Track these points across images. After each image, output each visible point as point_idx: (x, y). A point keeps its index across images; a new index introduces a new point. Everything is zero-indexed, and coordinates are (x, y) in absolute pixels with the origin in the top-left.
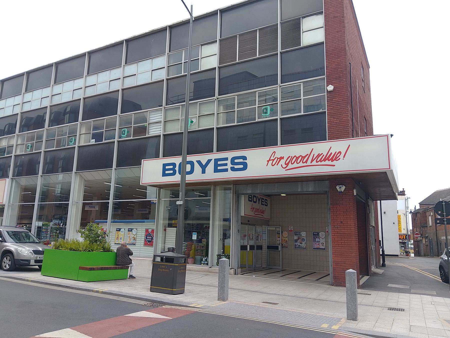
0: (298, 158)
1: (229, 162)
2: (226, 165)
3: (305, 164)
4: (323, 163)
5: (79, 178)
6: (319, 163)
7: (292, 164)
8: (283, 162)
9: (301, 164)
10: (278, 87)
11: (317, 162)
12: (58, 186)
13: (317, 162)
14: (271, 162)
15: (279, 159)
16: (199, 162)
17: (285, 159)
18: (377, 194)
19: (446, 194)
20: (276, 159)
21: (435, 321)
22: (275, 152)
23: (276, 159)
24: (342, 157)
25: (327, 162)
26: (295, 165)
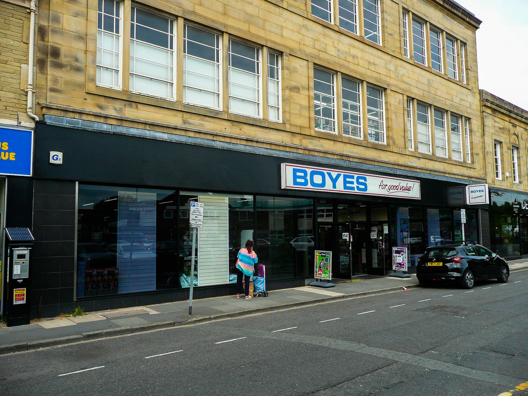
0: (394, 187)
1: (355, 180)
2: (352, 183)
3: (397, 191)
4: (405, 191)
5: (175, 192)
6: (403, 191)
7: (392, 190)
8: (387, 187)
9: (396, 190)
10: (360, 137)
11: (402, 190)
12: (473, 281)
13: (402, 190)
14: (381, 186)
15: (385, 186)
16: (329, 175)
17: (388, 186)
18: (185, 250)
19: (209, 242)
20: (384, 185)
21: (491, 167)
22: (382, 181)
23: (384, 185)
24: (411, 189)
25: (406, 191)
26: (393, 191)
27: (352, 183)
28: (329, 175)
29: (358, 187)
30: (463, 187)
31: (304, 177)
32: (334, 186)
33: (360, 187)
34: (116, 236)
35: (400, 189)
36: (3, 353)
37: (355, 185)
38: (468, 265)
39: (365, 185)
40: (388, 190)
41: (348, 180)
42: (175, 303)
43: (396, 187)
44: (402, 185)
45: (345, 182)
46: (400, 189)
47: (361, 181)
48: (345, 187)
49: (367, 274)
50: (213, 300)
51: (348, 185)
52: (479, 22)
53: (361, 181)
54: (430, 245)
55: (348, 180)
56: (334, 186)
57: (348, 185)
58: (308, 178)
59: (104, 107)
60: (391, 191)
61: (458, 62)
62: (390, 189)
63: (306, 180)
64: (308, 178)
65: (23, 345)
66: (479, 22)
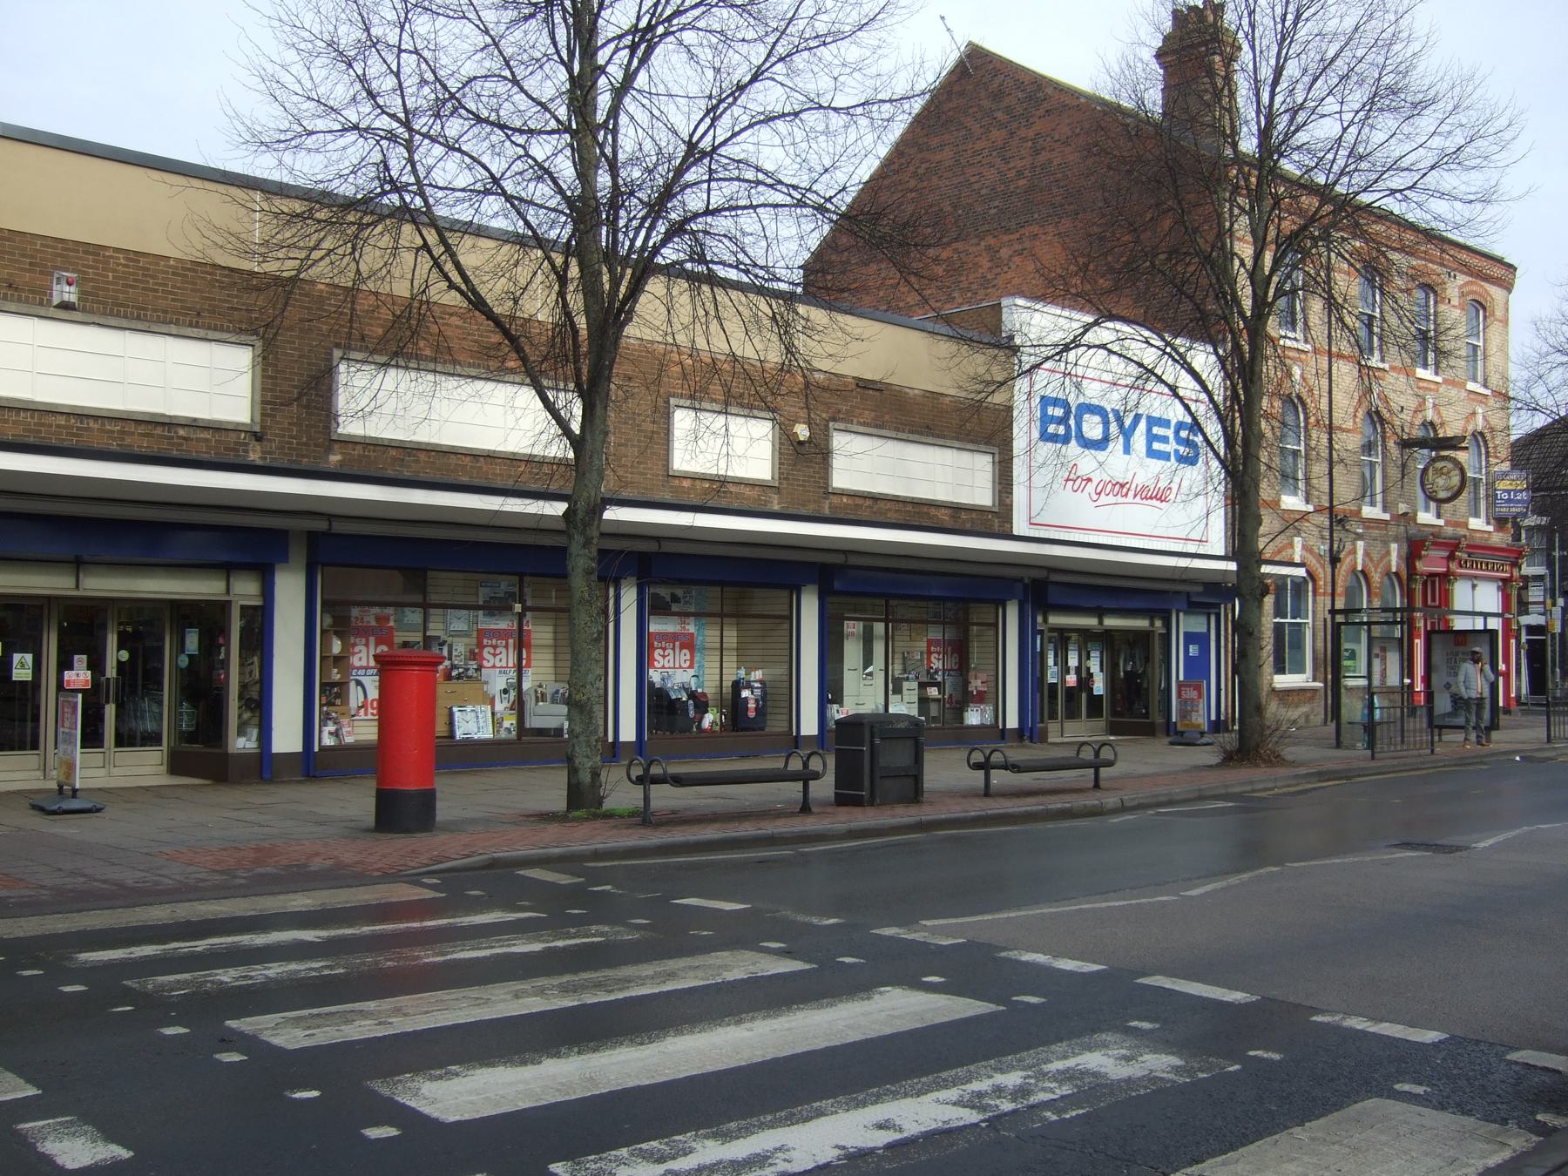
1: (1170, 433)
2: (1165, 440)
6: (1145, 502)
8: (1091, 487)
17: (1095, 481)
23: (1079, 480)
24: (1172, 497)
25: (1154, 502)
27: (1165, 440)
35: (1135, 496)
36: (1082, 100)
38: (280, 1051)
41: (1155, 430)
45: (1151, 438)
46: (1135, 496)
49: (163, 639)
50: (590, 1090)
51: (1156, 446)
52: (1515, 269)
55: (1155, 430)
57: (1156, 446)
59: (1493, 183)
63: (1068, 427)
64: (1072, 422)
66: (1511, 268)
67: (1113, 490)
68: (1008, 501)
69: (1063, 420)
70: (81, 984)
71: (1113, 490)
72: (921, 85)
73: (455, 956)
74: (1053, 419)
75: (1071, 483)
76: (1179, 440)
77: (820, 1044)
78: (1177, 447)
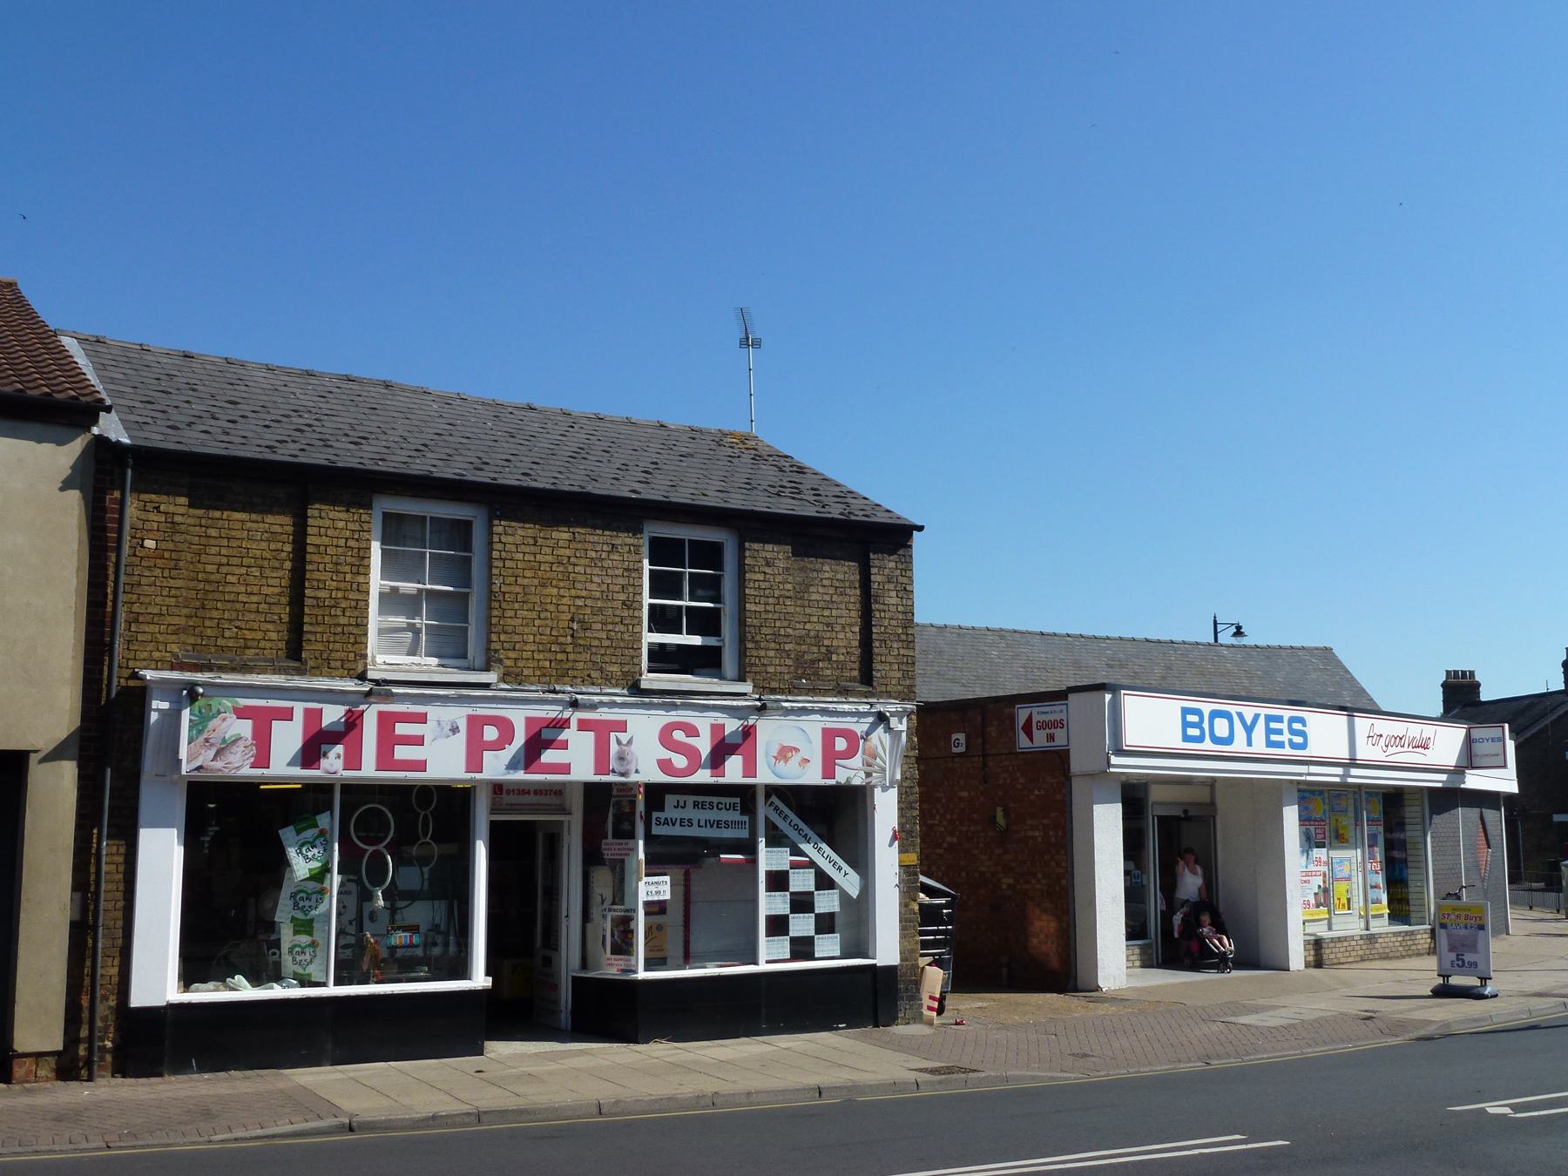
1: (1284, 726)
2: (1280, 732)
3: (1402, 749)
6: (1415, 750)
8: (1382, 740)
17: (1385, 737)
24: (1431, 745)
26: (1394, 750)
27: (1280, 732)
28: (1240, 715)
29: (1290, 741)
30: (1503, 727)
31: (1199, 725)
32: (1250, 744)
33: (1294, 741)
34: (590, 788)
37: (1286, 737)
39: (1303, 734)
40: (1385, 749)
41: (1273, 725)
42: (462, 1061)
43: (1401, 739)
44: (1411, 734)
45: (1269, 731)
47: (1296, 726)
48: (1270, 744)
51: (1274, 738)
53: (1296, 726)
54: (436, 906)
55: (1273, 725)
56: (1250, 744)
57: (1274, 738)
58: (1206, 725)
60: (1391, 750)
61: (742, 581)
62: (1387, 746)
63: (1202, 731)
64: (1206, 725)
65: (385, 1120)
67: (1395, 741)
68: (1132, 866)
69: (1199, 725)
70: (741, 854)
71: (1395, 741)
72: (476, 1104)
73: (611, 809)
74: (1193, 725)
75: (1370, 739)
76: (1293, 732)
77: (367, 994)
78: (1304, 729)
